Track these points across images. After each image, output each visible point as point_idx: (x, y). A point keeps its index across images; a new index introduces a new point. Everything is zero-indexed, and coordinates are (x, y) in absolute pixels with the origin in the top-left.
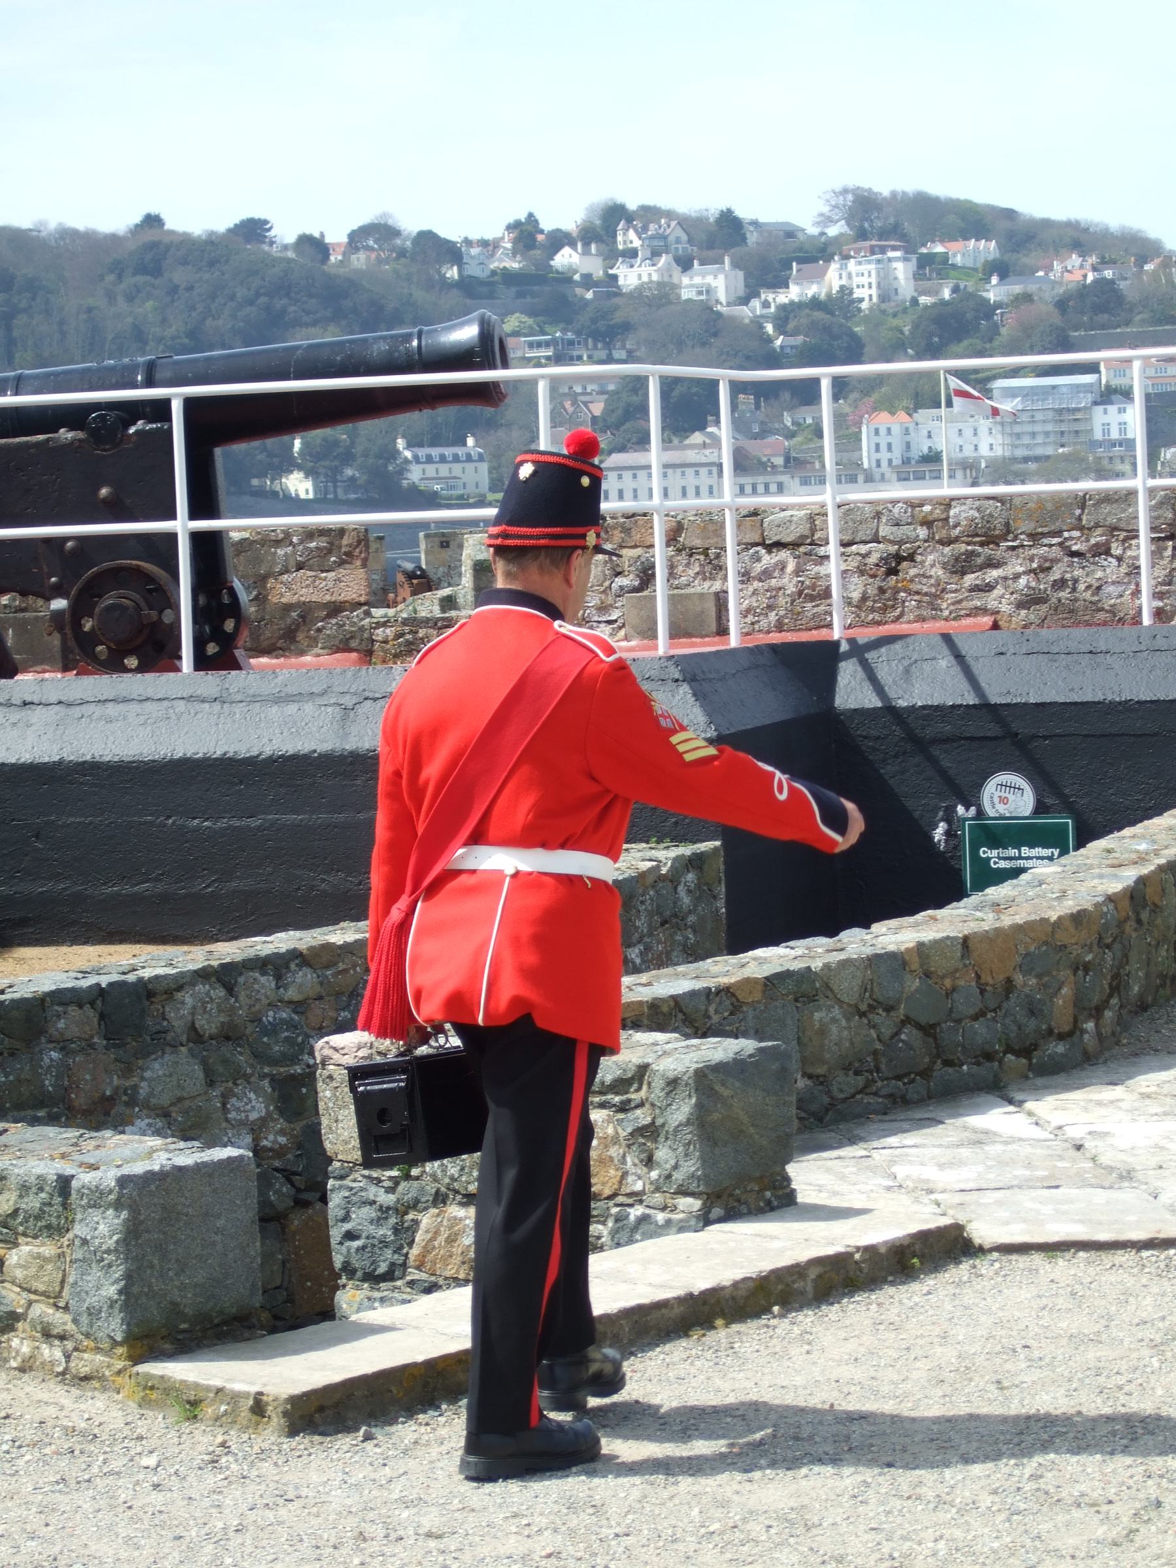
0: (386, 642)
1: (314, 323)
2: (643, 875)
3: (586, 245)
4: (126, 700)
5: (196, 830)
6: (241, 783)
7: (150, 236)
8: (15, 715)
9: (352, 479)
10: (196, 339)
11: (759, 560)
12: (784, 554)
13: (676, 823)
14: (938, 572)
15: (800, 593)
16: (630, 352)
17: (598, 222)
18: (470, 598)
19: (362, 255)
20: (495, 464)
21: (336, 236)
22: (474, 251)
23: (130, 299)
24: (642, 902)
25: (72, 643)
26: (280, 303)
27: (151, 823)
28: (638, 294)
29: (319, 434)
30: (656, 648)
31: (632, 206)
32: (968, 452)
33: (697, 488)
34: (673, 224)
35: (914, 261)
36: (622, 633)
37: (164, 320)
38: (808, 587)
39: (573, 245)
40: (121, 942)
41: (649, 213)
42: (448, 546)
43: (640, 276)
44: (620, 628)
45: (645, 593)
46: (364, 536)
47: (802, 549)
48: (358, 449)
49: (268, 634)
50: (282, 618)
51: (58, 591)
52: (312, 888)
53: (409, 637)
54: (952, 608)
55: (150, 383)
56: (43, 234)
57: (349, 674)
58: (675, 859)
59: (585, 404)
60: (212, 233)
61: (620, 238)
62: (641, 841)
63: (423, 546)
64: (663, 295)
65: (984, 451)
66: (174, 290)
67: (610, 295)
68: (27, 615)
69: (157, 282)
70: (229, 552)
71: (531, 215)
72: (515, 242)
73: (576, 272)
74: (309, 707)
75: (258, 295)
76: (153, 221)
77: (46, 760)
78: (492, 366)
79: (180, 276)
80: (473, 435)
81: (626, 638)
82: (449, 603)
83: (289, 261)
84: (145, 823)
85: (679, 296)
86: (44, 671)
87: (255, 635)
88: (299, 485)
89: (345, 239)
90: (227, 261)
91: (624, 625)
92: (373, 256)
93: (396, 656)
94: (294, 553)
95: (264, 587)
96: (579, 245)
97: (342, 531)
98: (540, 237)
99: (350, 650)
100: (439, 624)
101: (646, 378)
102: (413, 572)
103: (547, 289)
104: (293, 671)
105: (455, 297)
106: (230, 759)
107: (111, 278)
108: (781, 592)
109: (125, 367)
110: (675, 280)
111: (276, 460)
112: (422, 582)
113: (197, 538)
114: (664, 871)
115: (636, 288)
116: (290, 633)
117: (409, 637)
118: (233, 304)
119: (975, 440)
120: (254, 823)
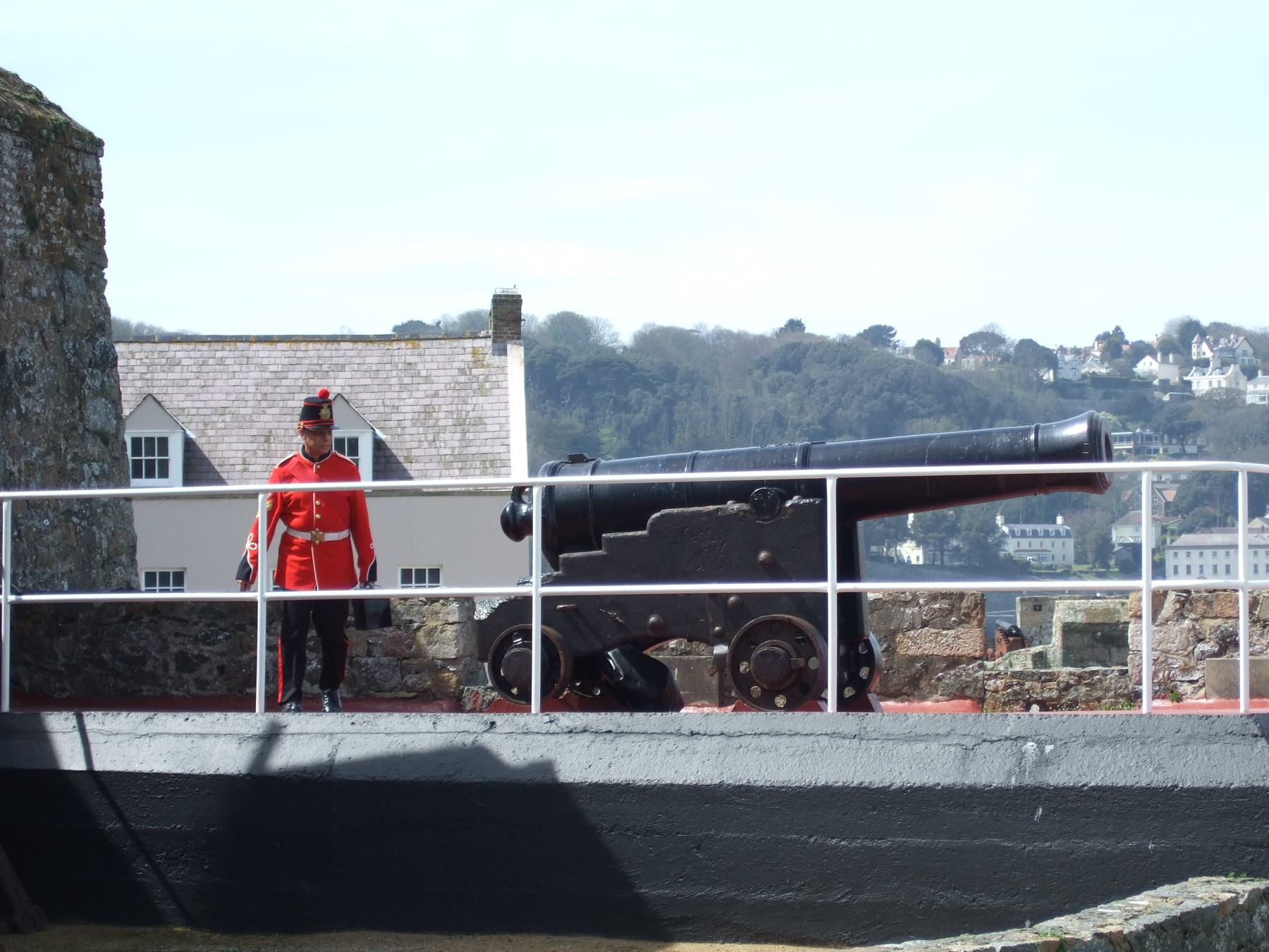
0: (996, 691)
1: (929, 415)
2: (1223, 905)
3: (1165, 355)
4: (778, 734)
5: (835, 847)
6: (874, 809)
7: (792, 338)
8: (684, 743)
9: (957, 549)
10: (829, 427)
13: (1252, 860)
16: (1200, 448)
17: (1176, 336)
18: (1059, 655)
19: (972, 359)
20: (1080, 540)
21: (950, 342)
22: (1068, 358)
23: (774, 390)
24: (1222, 929)
25: (729, 681)
26: (900, 398)
27: (796, 841)
28: (1209, 398)
29: (928, 514)
30: (1237, 706)
31: (1205, 322)
33: (1189, 567)
34: (1241, 339)
36: (1202, 691)
37: (801, 410)
39: (1153, 353)
40: (766, 942)
41: (1220, 330)
42: (1040, 609)
43: (1211, 383)
44: (1201, 687)
45: (1224, 658)
46: (982, 601)
48: (963, 524)
49: (895, 681)
50: (907, 668)
51: (720, 638)
52: (932, 902)
55: (805, 464)
56: (703, 334)
57: (970, 719)
58: (1251, 892)
59: (1160, 491)
60: (845, 337)
61: (1194, 350)
62: (1220, 874)
63: (1018, 609)
64: (1229, 400)
66: (810, 384)
67: (1183, 398)
68: (691, 657)
69: (796, 377)
70: (866, 609)
71: (1118, 328)
72: (1104, 351)
73: (1155, 377)
74: (934, 746)
75: (881, 390)
76: (795, 325)
77: (709, 782)
78: (1098, 459)
79: (816, 372)
80: (1062, 514)
81: (1206, 696)
82: (1040, 659)
83: (909, 362)
84: (791, 840)
85: (1244, 401)
86: (703, 706)
87: (884, 683)
88: (911, 552)
89: (958, 345)
90: (856, 361)
92: (981, 360)
93: (1005, 704)
94: (920, 612)
95: (894, 640)
96: (1159, 355)
97: (962, 595)
98: (1125, 348)
99: (965, 698)
101: (1237, 474)
102: (1010, 631)
103: (1130, 391)
104: (922, 714)
105: (1049, 398)
106: (865, 788)
107: (759, 372)
109: (785, 451)
110: (1241, 387)
111: (892, 531)
112: (1017, 639)
113: (843, 598)
114: (1241, 902)
115: (1207, 393)
116: (914, 681)
118: (860, 398)
120: (885, 844)
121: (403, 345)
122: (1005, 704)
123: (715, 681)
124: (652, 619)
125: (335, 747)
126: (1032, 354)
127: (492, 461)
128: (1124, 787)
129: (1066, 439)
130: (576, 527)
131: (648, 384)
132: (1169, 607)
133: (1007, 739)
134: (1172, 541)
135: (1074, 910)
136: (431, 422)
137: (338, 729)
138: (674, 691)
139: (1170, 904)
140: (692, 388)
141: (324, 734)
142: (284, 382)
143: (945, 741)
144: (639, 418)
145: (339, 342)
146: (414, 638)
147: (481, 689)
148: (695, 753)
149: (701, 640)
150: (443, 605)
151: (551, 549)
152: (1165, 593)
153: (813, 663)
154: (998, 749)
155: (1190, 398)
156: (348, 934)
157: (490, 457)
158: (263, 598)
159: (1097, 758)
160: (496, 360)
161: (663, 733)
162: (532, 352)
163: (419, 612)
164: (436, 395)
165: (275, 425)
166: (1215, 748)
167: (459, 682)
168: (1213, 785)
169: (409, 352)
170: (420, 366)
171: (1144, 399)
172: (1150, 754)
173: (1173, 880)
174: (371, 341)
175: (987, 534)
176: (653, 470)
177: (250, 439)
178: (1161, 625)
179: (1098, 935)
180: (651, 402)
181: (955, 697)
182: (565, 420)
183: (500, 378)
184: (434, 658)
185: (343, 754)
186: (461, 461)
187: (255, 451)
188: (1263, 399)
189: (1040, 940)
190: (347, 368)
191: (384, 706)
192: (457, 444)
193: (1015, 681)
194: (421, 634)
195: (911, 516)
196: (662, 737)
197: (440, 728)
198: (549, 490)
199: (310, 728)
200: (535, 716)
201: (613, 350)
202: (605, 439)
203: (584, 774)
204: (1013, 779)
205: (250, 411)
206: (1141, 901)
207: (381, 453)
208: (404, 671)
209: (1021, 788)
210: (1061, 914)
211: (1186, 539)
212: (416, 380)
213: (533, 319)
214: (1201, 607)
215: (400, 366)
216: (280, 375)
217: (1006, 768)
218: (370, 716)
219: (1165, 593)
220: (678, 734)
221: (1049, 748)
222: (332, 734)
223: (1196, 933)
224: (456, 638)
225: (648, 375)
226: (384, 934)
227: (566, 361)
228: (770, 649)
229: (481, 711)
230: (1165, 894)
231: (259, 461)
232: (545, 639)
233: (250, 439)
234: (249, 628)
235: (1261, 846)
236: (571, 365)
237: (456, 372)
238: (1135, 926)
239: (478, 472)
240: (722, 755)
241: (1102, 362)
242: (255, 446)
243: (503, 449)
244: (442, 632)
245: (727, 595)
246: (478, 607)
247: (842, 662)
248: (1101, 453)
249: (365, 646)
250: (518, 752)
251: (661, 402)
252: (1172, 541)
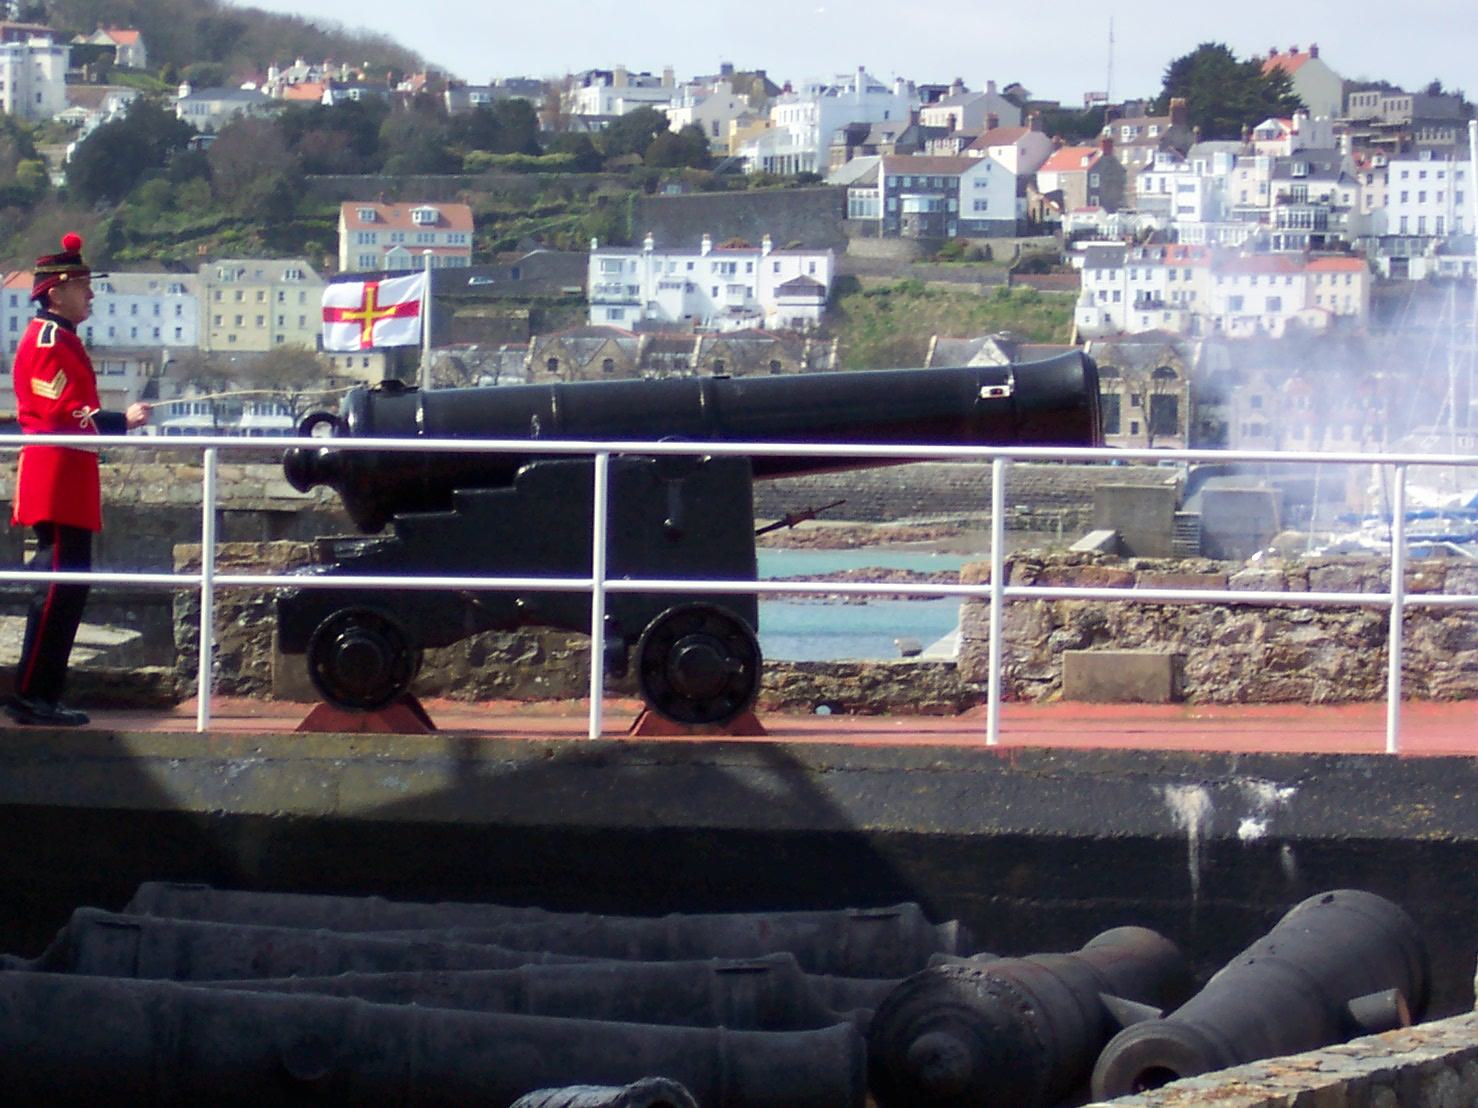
0: (775, 688)
11: (1222, 621)
12: (1252, 617)
14: (1428, 647)
15: (1268, 660)
32: (145, 339)
35: (66, 54)
38: (1277, 655)
47: (1272, 612)
53: (803, 684)
54: (1440, 687)
65: (168, 338)
91: (1060, 685)
100: (841, 671)
108: (1245, 660)
117: (803, 684)
119: (155, 323)
120: (1088, 904)
193: (801, 674)
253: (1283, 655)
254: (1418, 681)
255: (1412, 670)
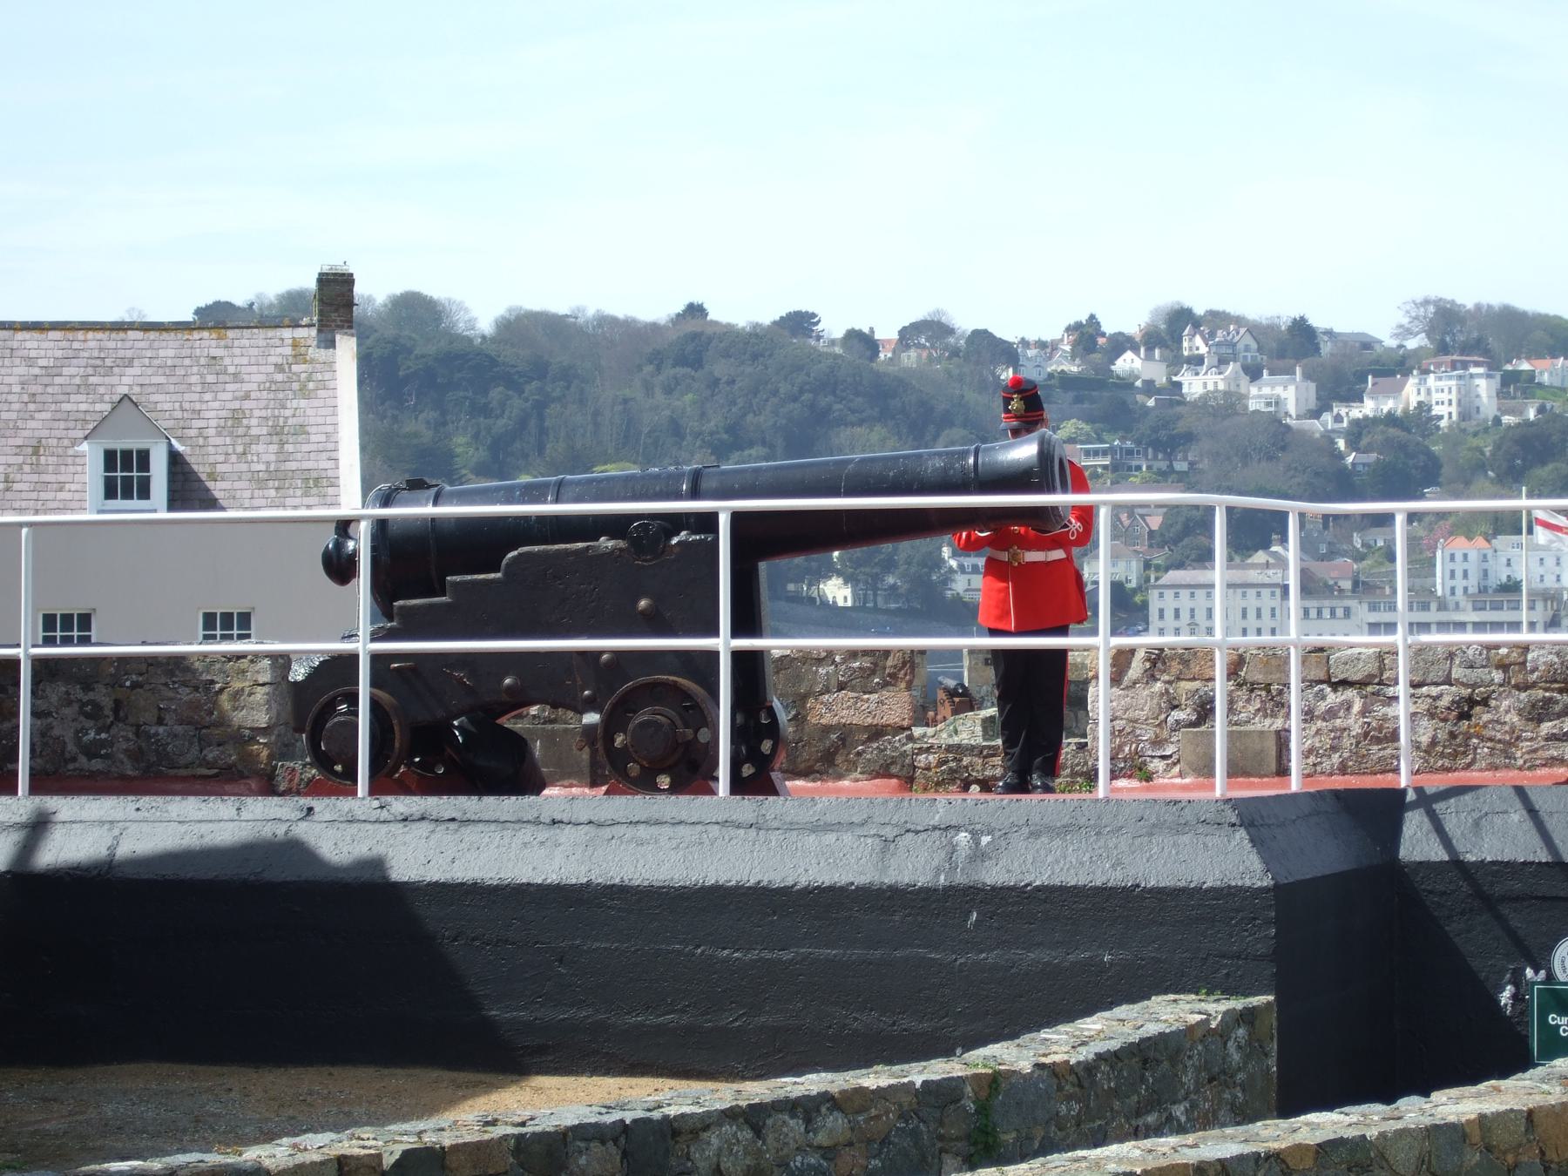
0: (928, 769)
1: (861, 423)
2: (1191, 1029)
3: (1150, 349)
4: (658, 823)
5: (726, 960)
6: (774, 913)
7: (692, 326)
8: (544, 834)
9: (893, 587)
10: (734, 439)
11: (1324, 698)
12: (1350, 693)
13: (1228, 975)
14: (1513, 718)
15: (1366, 734)
16: (1192, 464)
19: (913, 353)
21: (887, 332)
22: (1031, 353)
23: (669, 391)
25: (602, 757)
26: (824, 401)
27: (679, 952)
28: (1203, 403)
30: (1213, 787)
31: (1199, 310)
34: (1242, 331)
36: (1176, 769)
37: (703, 414)
39: (1136, 350)
41: (1218, 319)
44: (1174, 764)
45: (1203, 728)
46: (912, 659)
47: (1370, 689)
49: (805, 756)
51: (590, 705)
55: (695, 494)
56: (581, 320)
58: (1226, 1013)
59: (1142, 516)
61: (1185, 344)
62: (1190, 992)
63: (966, 663)
64: (1227, 406)
67: (1172, 404)
68: (557, 726)
70: (769, 669)
71: (1092, 317)
72: (1075, 345)
73: (1137, 378)
74: (847, 838)
75: (801, 391)
76: (695, 311)
77: (574, 881)
78: (1050, 489)
79: (721, 369)
81: (1181, 775)
83: (836, 356)
85: (1246, 407)
86: (571, 786)
87: (792, 759)
88: (837, 591)
92: (925, 354)
93: (938, 784)
95: (804, 707)
97: (886, 653)
98: (1101, 341)
99: (891, 776)
102: (955, 689)
103: (1106, 394)
106: (763, 888)
107: (649, 368)
109: (670, 476)
110: (1243, 390)
113: (738, 657)
116: (830, 755)
118: (775, 400)
120: (787, 956)
121: (205, 334)
122: (938, 784)
123: (585, 755)
124: (507, 681)
125: (115, 838)
126: (987, 346)
127: (317, 480)
128: (1075, 887)
129: (1012, 464)
130: (411, 569)
131: (511, 381)
132: (1136, 668)
133: (935, 828)
134: (1157, 579)
135: (1013, 1036)
136: (241, 431)
137: (119, 815)
138: (534, 767)
139: (1127, 1029)
140: (568, 388)
141: (102, 823)
142: (58, 380)
143: (859, 831)
144: (501, 424)
145: (125, 330)
146: (215, 703)
147: (298, 765)
148: (558, 845)
149: (568, 707)
150: (252, 661)
151: (384, 592)
152: (1132, 651)
153: (704, 735)
154: (924, 841)
155: (1179, 403)
156: (133, 1067)
157: (314, 474)
158: (26, 654)
159: (1043, 852)
160: (322, 354)
161: (519, 821)
162: (369, 342)
163: (221, 671)
164: (247, 397)
165: (45, 433)
166: (1186, 839)
167: (271, 757)
168: (1182, 884)
169: (214, 343)
170: (227, 361)
171: (1124, 403)
172: (1106, 847)
173: (1132, 1000)
174: (166, 330)
175: (932, 569)
176: (509, 501)
177: (15, 450)
178: (1127, 688)
179: (1039, 1066)
180: (517, 404)
181: (878, 775)
182: (410, 426)
183: (327, 376)
184: (240, 727)
185: (125, 850)
186: (277, 479)
187: (20, 466)
188: (1269, 404)
189: (970, 1072)
190: (136, 362)
191: (178, 786)
192: (273, 458)
193: (951, 756)
194: (224, 696)
195: (836, 554)
196: (517, 826)
197: (245, 815)
198: (381, 525)
199: (84, 815)
200: (362, 801)
201: (470, 340)
202: (459, 450)
203: (422, 871)
204: (942, 877)
205: (14, 416)
206: (1092, 1024)
207: (179, 469)
208: (204, 743)
209: (951, 888)
210: (996, 1040)
211: (1173, 576)
212: (222, 378)
213: (370, 300)
214: (1175, 667)
215: (203, 361)
216: (52, 372)
217: (935, 863)
218: (159, 800)
219: (1132, 651)
220: (537, 822)
221: (985, 840)
222: (111, 822)
223: (1159, 1062)
224: (268, 702)
225: (513, 371)
226: (175, 1067)
227: (410, 351)
228: (651, 717)
229: (298, 793)
230: (1123, 1016)
231: (25, 478)
232: (375, 705)
233: (15, 450)
234: (11, 690)
235: (1238, 958)
236: (417, 358)
237: (271, 369)
238: (1085, 1054)
239: (299, 492)
240: (590, 849)
241: (1073, 358)
242: (20, 459)
243: (330, 464)
244: (250, 694)
245: (597, 654)
246: (294, 666)
247: (737, 734)
248: (1053, 480)
249: (155, 711)
250: (340, 845)
251: (528, 404)
252: (1157, 579)
253: (1380, 729)
254: (1504, 751)
255: (1500, 741)
